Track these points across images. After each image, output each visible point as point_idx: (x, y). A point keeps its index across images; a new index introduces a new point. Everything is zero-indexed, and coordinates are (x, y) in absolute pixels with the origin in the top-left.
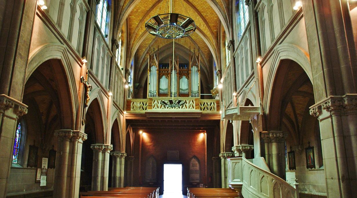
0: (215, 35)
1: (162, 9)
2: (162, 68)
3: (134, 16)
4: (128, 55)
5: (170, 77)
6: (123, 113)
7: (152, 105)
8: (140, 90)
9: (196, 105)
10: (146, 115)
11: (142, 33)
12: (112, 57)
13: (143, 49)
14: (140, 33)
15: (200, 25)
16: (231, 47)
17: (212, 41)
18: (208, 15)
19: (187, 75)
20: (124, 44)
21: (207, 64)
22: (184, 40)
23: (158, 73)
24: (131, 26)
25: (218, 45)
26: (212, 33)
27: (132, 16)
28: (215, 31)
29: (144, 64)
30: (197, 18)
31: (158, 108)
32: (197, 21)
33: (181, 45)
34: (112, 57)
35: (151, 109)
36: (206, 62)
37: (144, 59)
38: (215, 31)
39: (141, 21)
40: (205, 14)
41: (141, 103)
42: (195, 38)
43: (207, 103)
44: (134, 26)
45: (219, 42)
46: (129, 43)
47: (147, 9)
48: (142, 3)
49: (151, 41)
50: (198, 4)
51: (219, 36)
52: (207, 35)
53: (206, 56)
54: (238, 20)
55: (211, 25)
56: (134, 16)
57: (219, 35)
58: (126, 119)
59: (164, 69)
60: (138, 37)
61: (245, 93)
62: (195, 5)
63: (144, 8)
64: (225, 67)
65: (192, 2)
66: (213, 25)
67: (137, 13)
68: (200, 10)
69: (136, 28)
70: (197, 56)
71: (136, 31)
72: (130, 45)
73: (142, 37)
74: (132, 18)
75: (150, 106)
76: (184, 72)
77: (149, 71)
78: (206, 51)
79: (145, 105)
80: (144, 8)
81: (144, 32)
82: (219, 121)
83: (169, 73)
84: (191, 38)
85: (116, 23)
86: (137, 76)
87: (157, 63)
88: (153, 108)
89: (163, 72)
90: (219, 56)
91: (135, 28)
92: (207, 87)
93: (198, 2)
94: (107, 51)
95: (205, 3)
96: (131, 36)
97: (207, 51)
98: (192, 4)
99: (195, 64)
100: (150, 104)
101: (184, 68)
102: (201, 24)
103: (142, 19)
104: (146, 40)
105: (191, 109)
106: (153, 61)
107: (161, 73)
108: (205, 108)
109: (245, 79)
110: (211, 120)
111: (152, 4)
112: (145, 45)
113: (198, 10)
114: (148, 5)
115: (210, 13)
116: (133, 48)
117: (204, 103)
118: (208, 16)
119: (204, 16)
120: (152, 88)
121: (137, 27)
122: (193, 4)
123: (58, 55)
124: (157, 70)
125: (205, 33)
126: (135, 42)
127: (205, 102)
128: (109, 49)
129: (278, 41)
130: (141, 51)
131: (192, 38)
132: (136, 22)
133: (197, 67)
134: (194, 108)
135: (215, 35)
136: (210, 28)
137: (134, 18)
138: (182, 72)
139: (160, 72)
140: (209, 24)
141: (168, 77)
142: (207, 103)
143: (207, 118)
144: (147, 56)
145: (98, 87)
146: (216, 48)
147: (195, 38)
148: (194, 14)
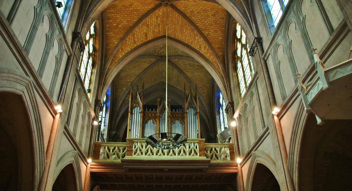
0: (221, 59)
1: (150, 27)
2: (148, 110)
3: (112, 33)
4: (101, 82)
5: (158, 122)
6: (86, 161)
7: (132, 151)
8: (117, 131)
9: (200, 151)
10: (122, 166)
11: (122, 56)
12: (71, 55)
13: (123, 89)
14: (120, 55)
15: (200, 47)
16: (229, 109)
17: (217, 67)
18: (211, 33)
19: (181, 120)
20: (97, 66)
21: (207, 108)
22: (177, 79)
23: (142, 116)
24: (108, 45)
25: (225, 71)
26: (217, 56)
27: (110, 33)
28: (220, 53)
29: (124, 109)
30: (196, 39)
31: (142, 154)
32: (196, 42)
33: (172, 86)
34: (71, 55)
35: (131, 155)
36: (205, 106)
37: (124, 101)
38: (220, 53)
39: (121, 39)
40: (207, 32)
41: (117, 148)
42: (191, 75)
43: (215, 149)
44: (112, 46)
45: (226, 67)
46: (104, 67)
47: (130, 25)
48: (125, 16)
49: (134, 79)
50: (198, 18)
51: (226, 60)
52: (210, 60)
53: (204, 99)
54: (265, 9)
55: (215, 46)
56: (112, 33)
57: (226, 58)
58: (91, 172)
59: (151, 111)
60: (117, 61)
61: (255, 157)
62: (194, 20)
63: (127, 23)
64: (239, 96)
65: (190, 16)
66: (218, 46)
67: (117, 29)
68: (200, 27)
69: (115, 48)
70: (194, 95)
71: (115, 52)
72: (104, 69)
73: (122, 60)
74: (110, 35)
75: (130, 152)
76: (177, 115)
77: (129, 114)
78: (205, 91)
79: (121, 151)
80: (127, 23)
81: (125, 55)
82: (235, 175)
83: (157, 117)
84: (186, 75)
85: (82, 13)
86: (114, 122)
87: (141, 104)
88: (135, 154)
89: (148, 115)
90: (228, 85)
91: (113, 48)
92: (209, 132)
93: (198, 17)
94: (64, 46)
95: (207, 18)
96: (107, 58)
97: (206, 91)
98: (189, 19)
99: (191, 106)
100: (129, 147)
101: (177, 110)
102: (202, 47)
103: (123, 37)
104: (128, 77)
105: (193, 155)
106: (136, 101)
107: (146, 116)
108: (212, 156)
109: (253, 141)
110: (223, 173)
111: (137, 18)
112: (126, 84)
113: (197, 27)
114: (131, 18)
115: (213, 31)
116: (109, 73)
117: (212, 149)
118: (211, 35)
119: (205, 34)
120: (134, 133)
121: (117, 46)
122: (192, 20)
123: (19, 89)
124: (141, 113)
125: (207, 57)
126: (112, 66)
127: (213, 147)
128: (68, 46)
129: (254, 148)
130: (120, 90)
131: (187, 74)
132: (116, 41)
133: (195, 109)
134: (197, 154)
135: (221, 59)
136: (214, 50)
137: (113, 35)
138: (174, 115)
139: (145, 115)
140: (212, 45)
141: (156, 121)
142: (215, 149)
143: (216, 170)
144: (127, 98)
145: (75, 150)
146: (223, 75)
147: (191, 75)
148: (192, 33)
